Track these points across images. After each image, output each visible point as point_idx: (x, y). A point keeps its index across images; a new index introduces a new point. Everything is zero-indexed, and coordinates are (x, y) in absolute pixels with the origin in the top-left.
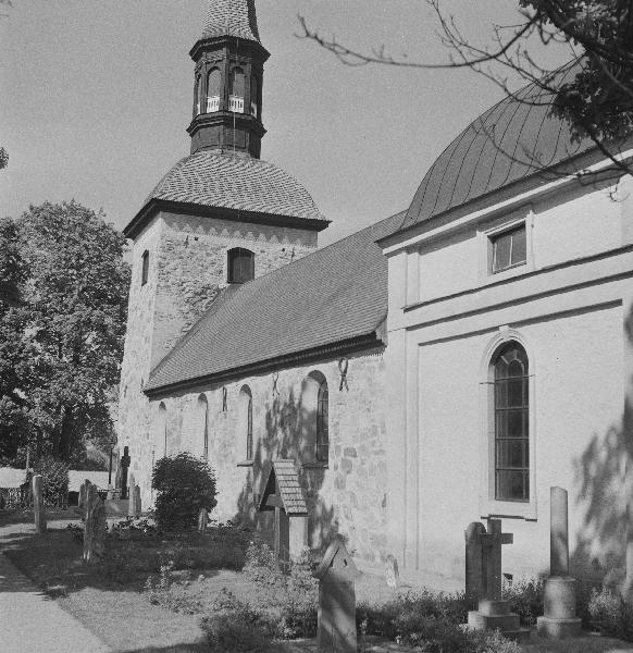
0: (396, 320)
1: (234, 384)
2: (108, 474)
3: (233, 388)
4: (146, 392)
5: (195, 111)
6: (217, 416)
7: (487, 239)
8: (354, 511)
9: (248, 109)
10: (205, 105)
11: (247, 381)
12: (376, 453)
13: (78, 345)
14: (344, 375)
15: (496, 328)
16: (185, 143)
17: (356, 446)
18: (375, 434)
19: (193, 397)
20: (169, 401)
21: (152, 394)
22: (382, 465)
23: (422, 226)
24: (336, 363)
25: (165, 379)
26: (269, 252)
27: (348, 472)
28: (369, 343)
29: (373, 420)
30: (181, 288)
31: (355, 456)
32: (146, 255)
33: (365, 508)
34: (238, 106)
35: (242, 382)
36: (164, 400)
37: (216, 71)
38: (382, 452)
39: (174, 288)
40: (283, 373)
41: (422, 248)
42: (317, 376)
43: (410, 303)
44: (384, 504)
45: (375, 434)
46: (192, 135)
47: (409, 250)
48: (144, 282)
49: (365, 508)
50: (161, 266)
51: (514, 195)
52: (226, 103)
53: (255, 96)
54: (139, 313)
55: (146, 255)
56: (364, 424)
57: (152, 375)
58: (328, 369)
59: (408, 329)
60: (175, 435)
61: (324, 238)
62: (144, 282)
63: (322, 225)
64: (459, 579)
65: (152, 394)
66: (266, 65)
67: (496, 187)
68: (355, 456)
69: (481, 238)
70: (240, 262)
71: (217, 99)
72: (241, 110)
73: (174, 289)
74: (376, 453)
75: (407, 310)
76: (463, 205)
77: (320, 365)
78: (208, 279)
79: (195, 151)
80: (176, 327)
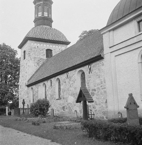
0: (106, 51)
1: (54, 78)
3: (53, 79)
5: (35, 16)
6: (49, 88)
7: (137, 22)
8: (96, 106)
9: (48, 15)
10: (38, 15)
11: (58, 77)
12: (102, 89)
13: (6, 77)
16: (33, 25)
17: (95, 88)
18: (102, 83)
19: (41, 84)
20: (34, 87)
21: (28, 86)
22: (105, 92)
24: (87, 66)
25: (30, 83)
26: (56, 49)
27: (94, 95)
28: (99, 58)
29: (101, 80)
30: (34, 59)
31: (95, 91)
32: (25, 52)
33: (100, 104)
34: (46, 14)
35: (57, 77)
37: (40, 6)
38: (105, 88)
39: (33, 59)
41: (114, 30)
43: (111, 46)
44: (106, 102)
45: (102, 83)
46: (34, 23)
47: (109, 31)
49: (100, 104)
51: (128, 17)
52: (43, 14)
53: (49, 12)
54: (23, 67)
55: (25, 52)
56: (98, 81)
58: (85, 69)
59: (111, 53)
60: (36, 95)
62: (24, 58)
64: (73, 95)
65: (28, 86)
66: (52, 5)
67: (115, 21)
68: (95, 91)
69: (135, 23)
70: (49, 52)
71: (41, 13)
72: (47, 16)
73: (33, 59)
74: (102, 89)
75: (110, 47)
76: (121, 19)
77: (82, 68)
78: (41, 57)
79: (35, 26)
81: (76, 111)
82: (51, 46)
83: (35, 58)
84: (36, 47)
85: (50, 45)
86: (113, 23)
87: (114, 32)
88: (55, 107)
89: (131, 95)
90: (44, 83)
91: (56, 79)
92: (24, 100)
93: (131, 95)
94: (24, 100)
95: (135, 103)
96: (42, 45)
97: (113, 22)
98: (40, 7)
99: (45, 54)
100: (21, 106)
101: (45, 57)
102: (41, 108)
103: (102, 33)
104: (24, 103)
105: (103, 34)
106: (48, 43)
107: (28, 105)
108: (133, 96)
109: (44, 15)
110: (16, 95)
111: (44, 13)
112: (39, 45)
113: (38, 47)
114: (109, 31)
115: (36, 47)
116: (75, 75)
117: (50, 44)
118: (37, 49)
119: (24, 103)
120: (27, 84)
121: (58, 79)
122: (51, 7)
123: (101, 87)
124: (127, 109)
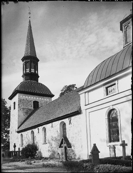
0: (83, 108)
1: (41, 127)
2: (16, 151)
3: (41, 128)
4: (17, 132)
9: (35, 71)
10: (26, 71)
11: (22, 133)
14: (70, 121)
15: (109, 106)
23: (90, 85)
25: (20, 129)
28: (78, 112)
32: (14, 103)
34: (33, 71)
35: (21, 133)
36: (39, 128)
38: (81, 136)
40: (54, 123)
42: (44, 128)
48: (14, 108)
50: (19, 105)
52: (30, 70)
53: (36, 68)
55: (14, 103)
57: (18, 128)
58: (66, 121)
61: (53, 99)
62: (14, 108)
63: (53, 96)
65: (18, 132)
71: (29, 69)
72: (34, 72)
73: (22, 110)
76: (94, 84)
78: (30, 108)
80: (23, 117)
81: (58, 153)
82: (38, 98)
83: (23, 109)
84: (25, 99)
85: (36, 98)
86: (95, 84)
87: (89, 93)
88: (44, 151)
89: (95, 145)
90: (33, 130)
91: (42, 128)
92: (15, 144)
93: (95, 145)
94: (15, 144)
95: (97, 150)
96: (30, 97)
97: (89, 85)
98: (28, 64)
99: (33, 105)
100: (12, 149)
101: (32, 108)
102: (30, 152)
103: (79, 94)
104: (15, 146)
105: (80, 94)
106: (35, 96)
107: (19, 149)
108: (96, 145)
109: (32, 71)
110: (6, 139)
111: (32, 69)
112: (27, 97)
113: (26, 99)
114: (85, 93)
115: (25, 99)
116: (57, 124)
117: (36, 96)
118: (26, 101)
119: (15, 146)
120: (17, 130)
121: (22, 135)
122: (38, 64)
123: (78, 135)
124: (92, 154)
